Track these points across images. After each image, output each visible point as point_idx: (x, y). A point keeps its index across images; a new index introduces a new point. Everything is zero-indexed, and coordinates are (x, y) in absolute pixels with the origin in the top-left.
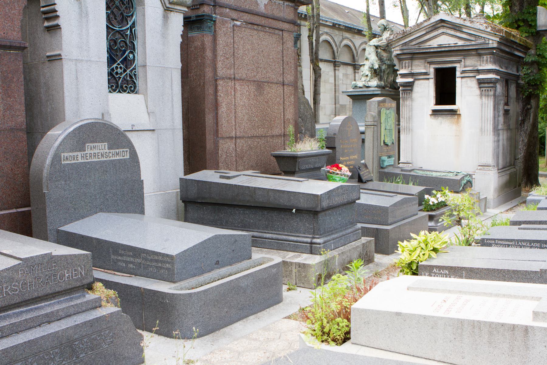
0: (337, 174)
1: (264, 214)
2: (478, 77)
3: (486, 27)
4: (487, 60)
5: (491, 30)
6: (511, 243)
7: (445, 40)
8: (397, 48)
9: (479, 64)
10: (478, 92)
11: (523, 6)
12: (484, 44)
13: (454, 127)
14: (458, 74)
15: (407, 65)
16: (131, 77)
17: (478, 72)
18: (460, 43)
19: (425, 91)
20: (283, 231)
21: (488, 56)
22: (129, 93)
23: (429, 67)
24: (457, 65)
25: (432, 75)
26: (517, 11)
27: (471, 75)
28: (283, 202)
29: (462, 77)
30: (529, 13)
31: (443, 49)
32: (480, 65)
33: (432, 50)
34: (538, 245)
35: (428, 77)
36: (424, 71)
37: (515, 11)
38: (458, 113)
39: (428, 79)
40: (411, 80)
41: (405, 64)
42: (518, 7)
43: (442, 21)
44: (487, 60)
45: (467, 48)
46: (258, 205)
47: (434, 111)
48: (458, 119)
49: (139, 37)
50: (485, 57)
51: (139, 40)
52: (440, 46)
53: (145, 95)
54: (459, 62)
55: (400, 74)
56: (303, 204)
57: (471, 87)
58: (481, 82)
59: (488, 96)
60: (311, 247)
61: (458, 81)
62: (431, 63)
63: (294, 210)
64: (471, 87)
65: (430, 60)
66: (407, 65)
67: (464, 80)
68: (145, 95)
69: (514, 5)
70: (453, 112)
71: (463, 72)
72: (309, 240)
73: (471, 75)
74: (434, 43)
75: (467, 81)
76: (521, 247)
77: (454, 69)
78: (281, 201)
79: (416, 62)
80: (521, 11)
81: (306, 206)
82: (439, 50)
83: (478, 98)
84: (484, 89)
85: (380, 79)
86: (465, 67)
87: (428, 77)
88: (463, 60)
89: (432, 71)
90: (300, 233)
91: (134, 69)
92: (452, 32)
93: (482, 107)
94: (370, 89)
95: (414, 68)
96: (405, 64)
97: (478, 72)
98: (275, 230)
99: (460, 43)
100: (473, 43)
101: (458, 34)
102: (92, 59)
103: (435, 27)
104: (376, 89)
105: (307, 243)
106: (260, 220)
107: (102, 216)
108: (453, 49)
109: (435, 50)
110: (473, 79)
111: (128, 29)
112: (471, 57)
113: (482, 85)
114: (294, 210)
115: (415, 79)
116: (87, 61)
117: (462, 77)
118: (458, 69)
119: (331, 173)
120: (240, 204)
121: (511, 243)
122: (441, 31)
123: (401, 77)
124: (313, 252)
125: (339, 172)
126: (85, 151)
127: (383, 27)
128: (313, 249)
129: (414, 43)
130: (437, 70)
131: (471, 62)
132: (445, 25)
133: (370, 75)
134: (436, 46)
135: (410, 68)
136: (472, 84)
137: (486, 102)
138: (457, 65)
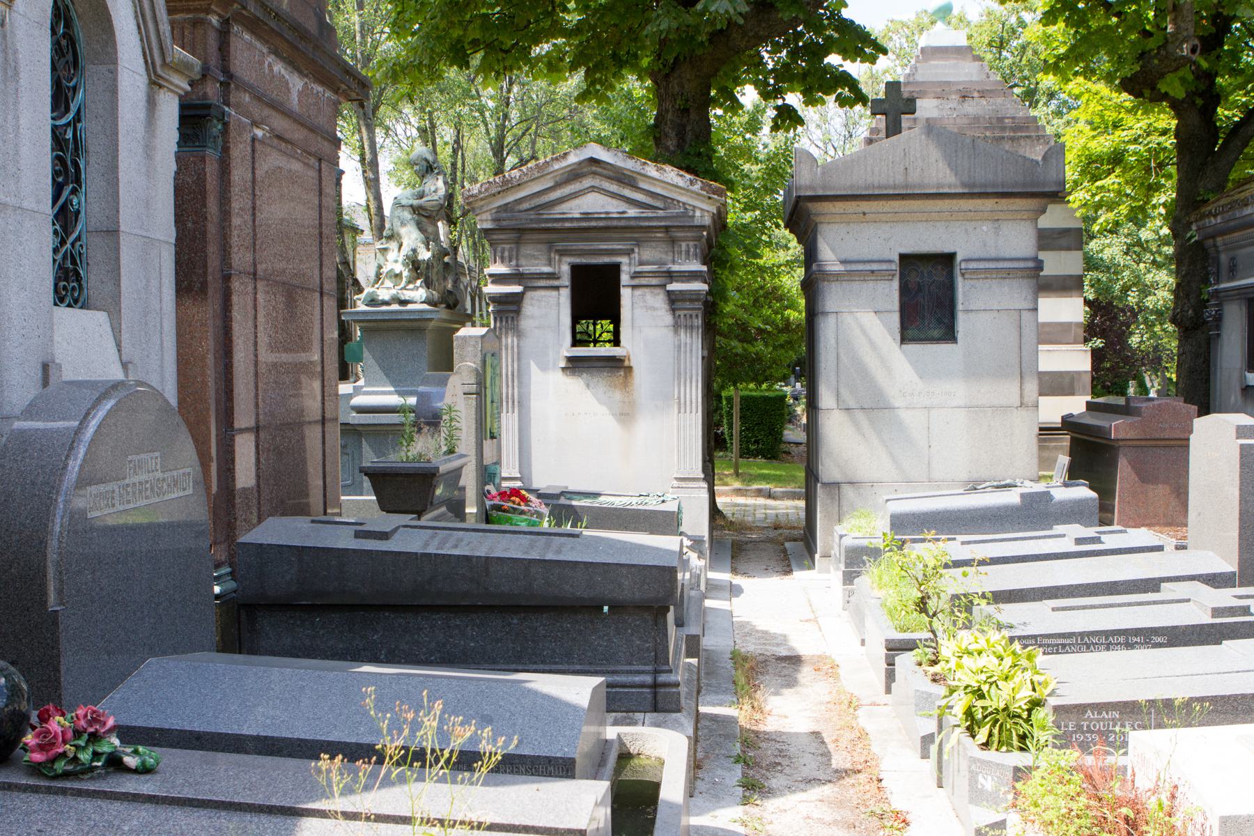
0: (522, 512)
1: (510, 624)
2: (670, 287)
3: (691, 182)
4: (688, 252)
5: (702, 189)
6: (1068, 641)
7: (594, 203)
8: (485, 216)
9: (670, 258)
10: (669, 319)
11: (684, 141)
12: (684, 215)
13: (617, 395)
14: (625, 278)
15: (506, 254)
16: (74, 262)
17: (671, 276)
18: (632, 212)
19: (550, 312)
20: (568, 663)
21: (691, 243)
22: (69, 306)
23: (560, 261)
24: (624, 260)
25: (566, 280)
26: (672, 148)
27: (654, 281)
28: (577, 589)
29: (634, 287)
30: (699, 154)
31: (593, 224)
32: (674, 262)
33: (567, 225)
34: (1121, 639)
35: (556, 283)
36: (547, 269)
37: (667, 149)
38: (626, 363)
39: (557, 288)
40: (517, 289)
41: (503, 252)
42: (674, 142)
43: (593, 161)
44: (688, 252)
45: (647, 224)
46: (497, 602)
47: (571, 359)
48: (626, 377)
49: (91, 149)
50: (684, 245)
51: (92, 159)
52: (587, 217)
53: (113, 308)
54: (628, 253)
55: (490, 275)
56: (629, 591)
57: (654, 309)
58: (674, 300)
59: (692, 327)
60: (655, 694)
61: (625, 293)
62: (563, 253)
63: (606, 609)
64: (654, 309)
65: (560, 245)
66: (506, 254)
67: (638, 292)
68: (113, 308)
69: (666, 136)
70: (616, 365)
71: (636, 275)
72: (648, 679)
73: (654, 281)
74: (574, 209)
75: (643, 296)
76: (1108, 649)
77: (616, 268)
78: (567, 587)
79: (527, 250)
80: (682, 150)
81: (637, 595)
82: (584, 224)
83: (669, 333)
84: (682, 313)
85: (428, 284)
86: (641, 263)
87: (556, 283)
88: (636, 250)
89: (565, 269)
90: (618, 662)
91: (79, 238)
92: (613, 187)
93: (679, 351)
94: (410, 307)
95: (523, 262)
96: (503, 252)
97: (671, 276)
98: (543, 662)
99: (632, 212)
100: (661, 213)
101: (627, 192)
102: (25, 204)
103: (574, 174)
104: (425, 307)
105: (642, 686)
106: (498, 641)
107: (153, 666)
108: (615, 223)
109: (575, 224)
110: (658, 291)
111: (69, 124)
112: (653, 244)
113: (679, 305)
114: (606, 609)
115: (527, 288)
116: (16, 208)
117: (634, 287)
118: (624, 268)
119: (504, 511)
120: (439, 602)
121: (1068, 641)
122: (587, 182)
123: (493, 282)
124: (660, 705)
125: (523, 507)
126: (124, 478)
127: (425, 163)
128: (659, 698)
129: (526, 206)
130: (576, 270)
131: (651, 254)
132: (599, 170)
133: (406, 273)
134: (578, 216)
135: (514, 263)
136: (658, 301)
137: (688, 341)
138: (624, 260)
